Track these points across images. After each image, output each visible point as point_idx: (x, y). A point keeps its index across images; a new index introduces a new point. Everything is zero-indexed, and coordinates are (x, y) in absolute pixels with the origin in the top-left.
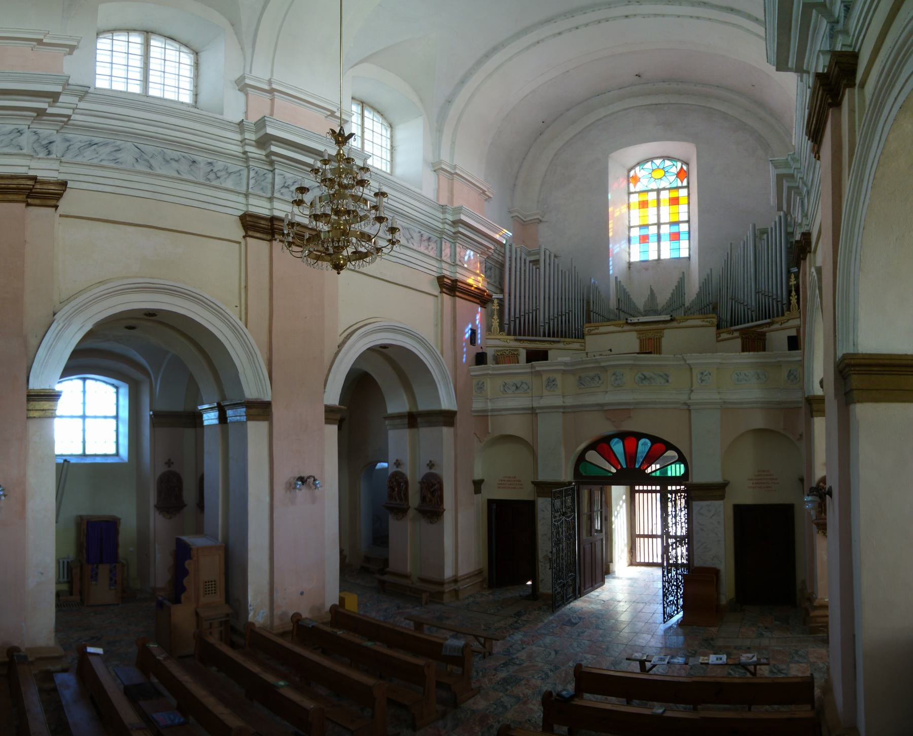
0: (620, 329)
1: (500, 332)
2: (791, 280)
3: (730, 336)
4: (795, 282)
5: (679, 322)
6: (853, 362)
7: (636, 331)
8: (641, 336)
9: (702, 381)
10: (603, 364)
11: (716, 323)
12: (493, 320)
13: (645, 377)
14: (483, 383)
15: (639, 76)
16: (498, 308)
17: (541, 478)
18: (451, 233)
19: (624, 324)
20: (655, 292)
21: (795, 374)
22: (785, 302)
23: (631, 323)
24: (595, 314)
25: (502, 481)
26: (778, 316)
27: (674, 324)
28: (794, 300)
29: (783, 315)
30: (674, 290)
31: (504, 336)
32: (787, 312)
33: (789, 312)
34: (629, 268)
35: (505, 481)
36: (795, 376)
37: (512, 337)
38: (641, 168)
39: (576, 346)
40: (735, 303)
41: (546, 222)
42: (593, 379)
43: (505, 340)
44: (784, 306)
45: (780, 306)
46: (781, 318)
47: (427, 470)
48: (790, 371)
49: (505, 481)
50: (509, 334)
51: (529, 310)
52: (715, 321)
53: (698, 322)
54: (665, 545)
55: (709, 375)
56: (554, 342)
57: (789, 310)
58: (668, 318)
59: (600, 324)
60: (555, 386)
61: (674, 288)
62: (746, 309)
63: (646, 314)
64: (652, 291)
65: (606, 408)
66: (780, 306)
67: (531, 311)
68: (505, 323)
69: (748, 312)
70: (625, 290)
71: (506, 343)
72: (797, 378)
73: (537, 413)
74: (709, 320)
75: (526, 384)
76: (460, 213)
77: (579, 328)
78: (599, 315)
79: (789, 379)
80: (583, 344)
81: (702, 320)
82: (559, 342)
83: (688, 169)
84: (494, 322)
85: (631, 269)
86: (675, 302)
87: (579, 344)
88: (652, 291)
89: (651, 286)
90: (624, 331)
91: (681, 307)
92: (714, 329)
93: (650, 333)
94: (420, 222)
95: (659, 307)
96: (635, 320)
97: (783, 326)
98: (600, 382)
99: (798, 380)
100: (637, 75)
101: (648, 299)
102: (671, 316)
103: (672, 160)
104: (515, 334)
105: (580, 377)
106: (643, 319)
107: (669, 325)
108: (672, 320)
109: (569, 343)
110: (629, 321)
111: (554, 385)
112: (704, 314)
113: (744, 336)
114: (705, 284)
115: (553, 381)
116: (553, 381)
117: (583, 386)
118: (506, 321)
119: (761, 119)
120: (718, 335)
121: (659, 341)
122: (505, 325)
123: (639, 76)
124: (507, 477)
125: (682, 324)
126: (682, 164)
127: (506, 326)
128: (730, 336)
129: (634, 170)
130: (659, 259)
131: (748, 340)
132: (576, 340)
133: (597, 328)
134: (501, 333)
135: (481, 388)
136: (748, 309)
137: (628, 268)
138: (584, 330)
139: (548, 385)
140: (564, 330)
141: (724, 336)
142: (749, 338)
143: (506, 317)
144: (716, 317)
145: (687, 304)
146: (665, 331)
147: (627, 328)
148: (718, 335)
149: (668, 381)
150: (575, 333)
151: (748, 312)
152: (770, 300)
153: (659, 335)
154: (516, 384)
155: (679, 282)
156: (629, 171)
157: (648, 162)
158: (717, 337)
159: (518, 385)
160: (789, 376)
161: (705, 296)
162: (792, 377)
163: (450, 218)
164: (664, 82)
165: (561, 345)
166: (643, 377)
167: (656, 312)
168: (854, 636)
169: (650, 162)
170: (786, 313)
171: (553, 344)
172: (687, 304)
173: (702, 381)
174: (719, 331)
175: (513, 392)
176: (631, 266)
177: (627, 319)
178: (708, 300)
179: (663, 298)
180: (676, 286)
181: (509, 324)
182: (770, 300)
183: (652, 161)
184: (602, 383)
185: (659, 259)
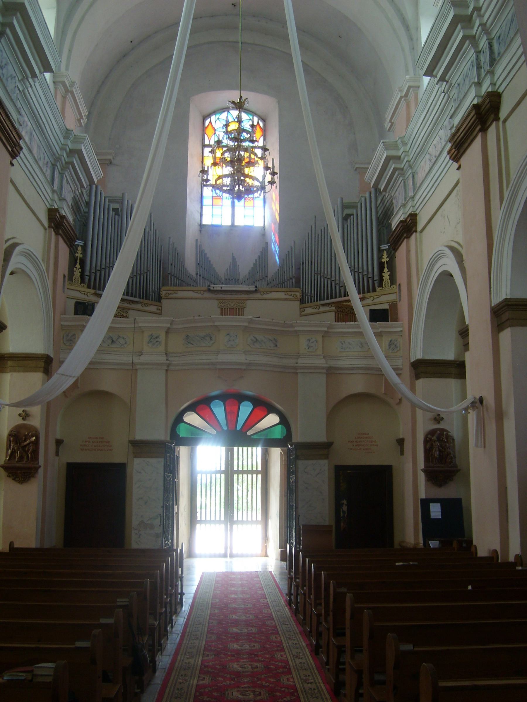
0: (199, 295)
1: (81, 283)
2: (383, 257)
3: (316, 310)
4: (388, 259)
5: (262, 293)
6: (510, 303)
7: (217, 299)
8: (223, 305)
9: (309, 347)
10: (216, 324)
11: (299, 297)
12: (75, 269)
13: (257, 339)
14: (74, 335)
15: (235, 6)
16: (81, 256)
17: (139, 437)
18: (64, 162)
19: (204, 291)
20: (235, 257)
21: (395, 344)
22: (376, 278)
23: (213, 290)
24: (173, 278)
25: (86, 442)
26: (369, 291)
27: (258, 295)
28: (386, 276)
29: (374, 290)
30: (256, 260)
31: (84, 289)
32: (379, 288)
33: (381, 288)
34: (200, 231)
35: (90, 442)
36: (396, 346)
37: (92, 291)
38: (217, 118)
39: (153, 309)
40: (321, 278)
41: (116, 165)
42: (203, 338)
43: (86, 293)
44: (375, 282)
45: (370, 282)
46: (371, 294)
47: (20, 421)
48: (391, 341)
49: (90, 442)
50: (89, 287)
51: (109, 264)
52: (299, 295)
53: (282, 295)
54: (175, 553)
55: (316, 342)
56: (133, 302)
57: (381, 285)
58: (252, 288)
59: (175, 288)
60: (158, 342)
61: (257, 258)
62: (333, 284)
63: (228, 281)
64: (233, 259)
65: (219, 367)
66: (370, 282)
67: (93, 271)
68: (86, 274)
69: (335, 287)
70: (205, 254)
71: (86, 297)
72: (397, 347)
73: (137, 370)
74: (293, 293)
75: (123, 338)
76: (82, 143)
77: (156, 290)
78: (177, 278)
79: (390, 348)
80: (160, 308)
81: (286, 293)
82: (137, 302)
83: (265, 125)
84: (76, 271)
85: (202, 232)
86: (257, 272)
87: (156, 307)
88: (233, 259)
89: (233, 253)
90: (205, 299)
91: (264, 278)
92: (298, 303)
93: (232, 302)
94: (428, 136)
95: (241, 277)
96: (218, 287)
97: (375, 301)
98: (212, 342)
99: (398, 349)
100: (233, 4)
101: (230, 267)
102: (256, 287)
103: (249, 113)
104: (94, 288)
105: (187, 336)
106: (225, 287)
107: (252, 296)
108: (256, 291)
109: (147, 305)
110: (212, 289)
111: (157, 342)
112: (290, 287)
113: (339, 310)
114: (285, 257)
115: (157, 338)
116: (157, 338)
117: (191, 345)
118: (87, 273)
119: (124, 56)
120: (301, 310)
121: (242, 311)
122: (86, 277)
123: (235, 6)
124: (94, 438)
125: (265, 296)
126: (259, 120)
127: (87, 278)
128: (316, 310)
129: (210, 119)
130: (233, 225)
131: (342, 313)
132: (153, 303)
133: (176, 292)
134: (82, 285)
135: (71, 340)
136: (336, 284)
137: (199, 232)
138: (161, 293)
139: (150, 341)
140: (130, 292)
141: (309, 310)
142: (343, 312)
143: (88, 268)
144: (300, 292)
145: (270, 275)
146: (249, 303)
147: (207, 295)
148: (302, 310)
149: (276, 346)
150: (152, 295)
151: (335, 287)
152: (361, 276)
153: (241, 305)
154: (112, 338)
155: (262, 252)
156: (205, 118)
157: (224, 111)
158: (301, 312)
159: (114, 339)
160: (390, 345)
161: (288, 269)
162: (392, 346)
163: (71, 146)
164: (254, 16)
165: (139, 306)
166: (255, 340)
167: (237, 282)
168: (506, 488)
169: (226, 112)
170: (378, 289)
171: (132, 304)
172: (270, 275)
173: (309, 347)
174: (304, 305)
175: (108, 345)
176: (203, 229)
177: (209, 286)
178: (288, 275)
179: (244, 269)
180: (259, 257)
181: (90, 276)
182: (361, 276)
183: (228, 112)
184: (214, 343)
185: (233, 225)
